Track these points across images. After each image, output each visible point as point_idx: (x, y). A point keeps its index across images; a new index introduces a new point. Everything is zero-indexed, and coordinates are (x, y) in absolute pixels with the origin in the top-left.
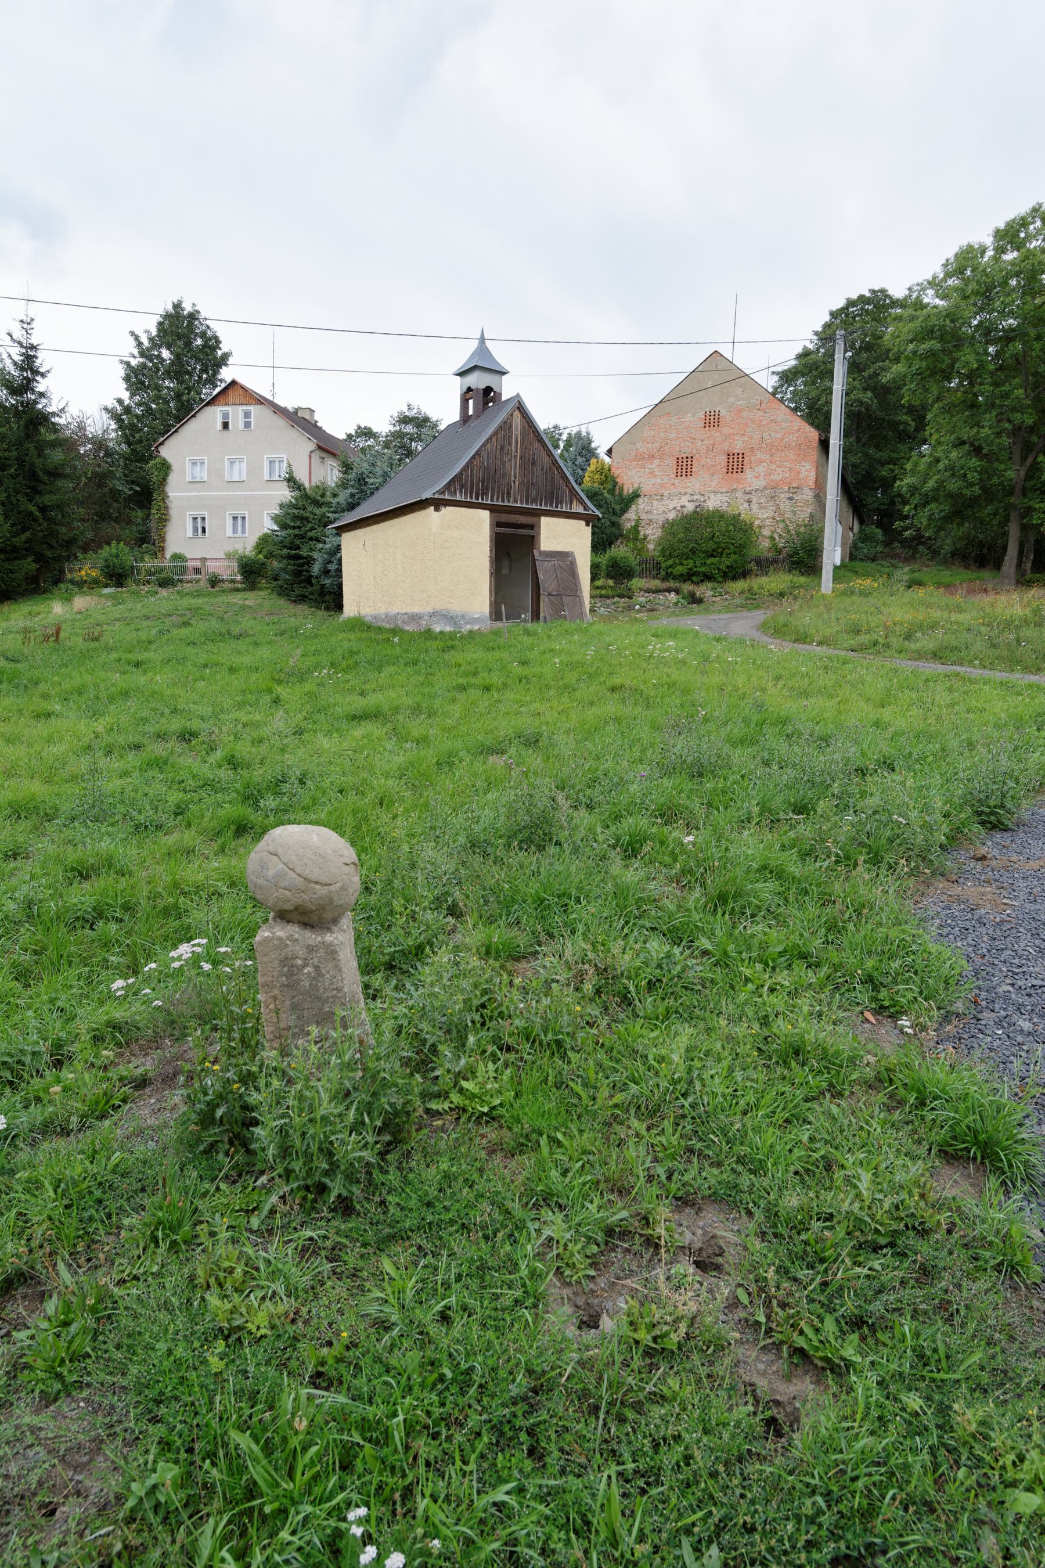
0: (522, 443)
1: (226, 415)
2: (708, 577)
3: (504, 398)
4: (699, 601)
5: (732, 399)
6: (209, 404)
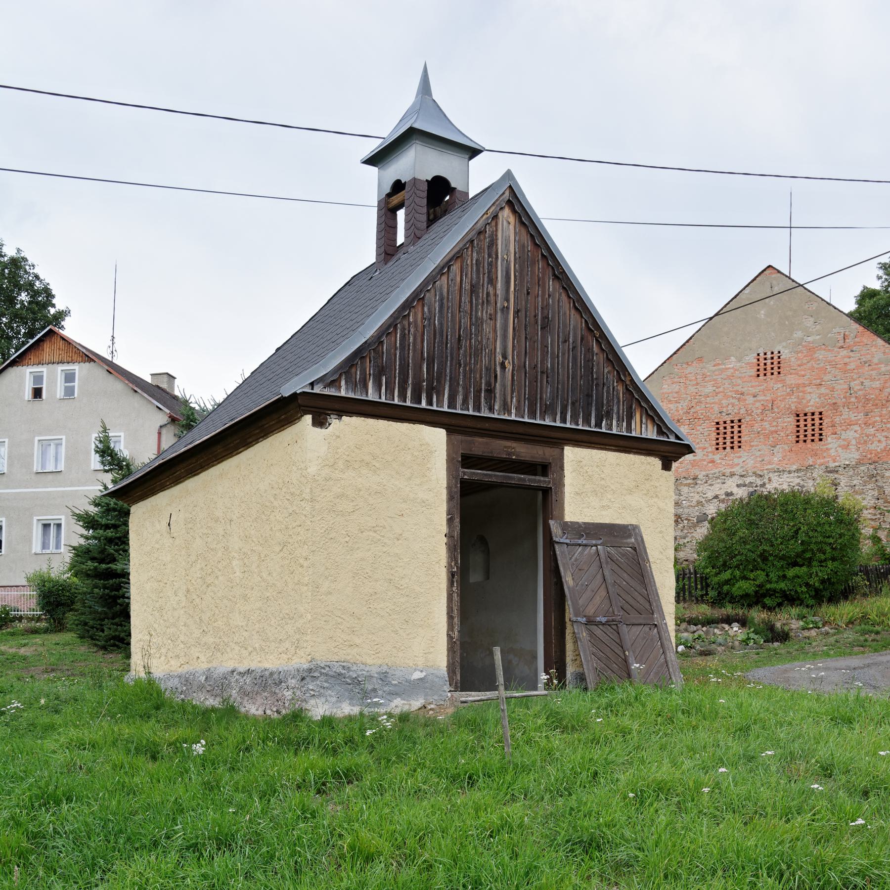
0: (520, 278)
1: (38, 378)
2: (790, 599)
3: (470, 196)
4: (783, 637)
5: (798, 334)
6: (14, 363)
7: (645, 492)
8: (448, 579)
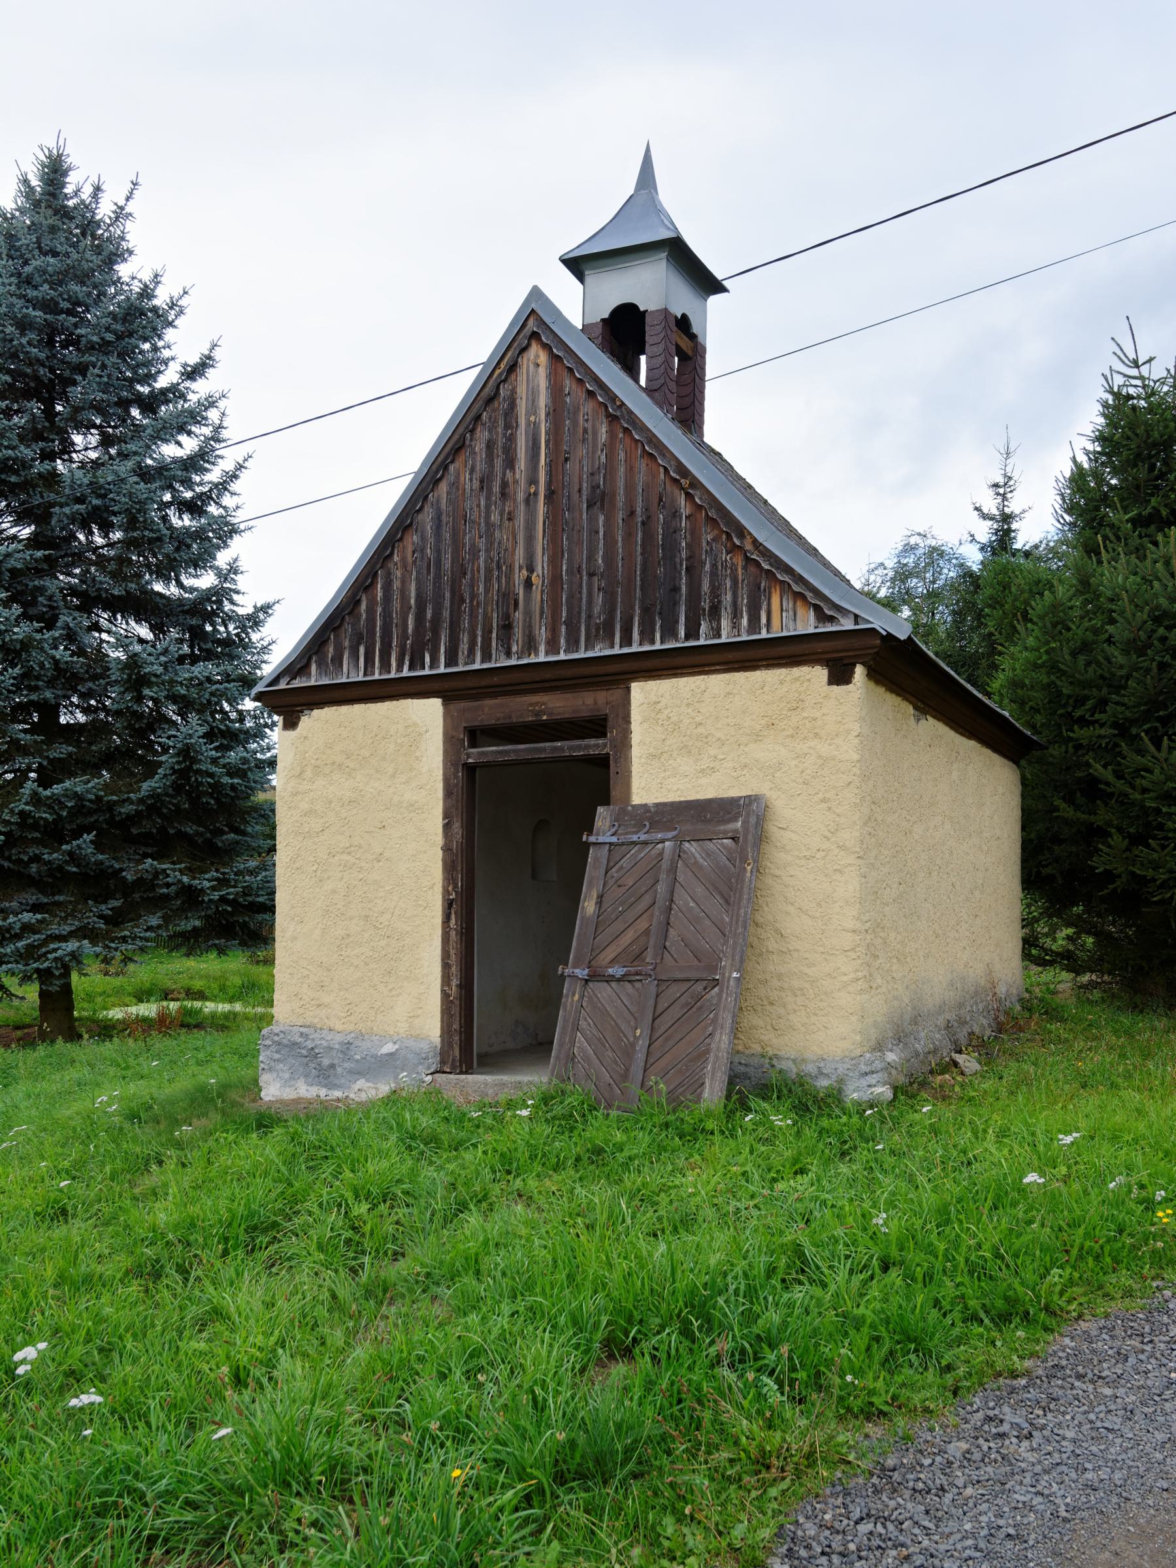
7: (791, 731)
8: (444, 911)
